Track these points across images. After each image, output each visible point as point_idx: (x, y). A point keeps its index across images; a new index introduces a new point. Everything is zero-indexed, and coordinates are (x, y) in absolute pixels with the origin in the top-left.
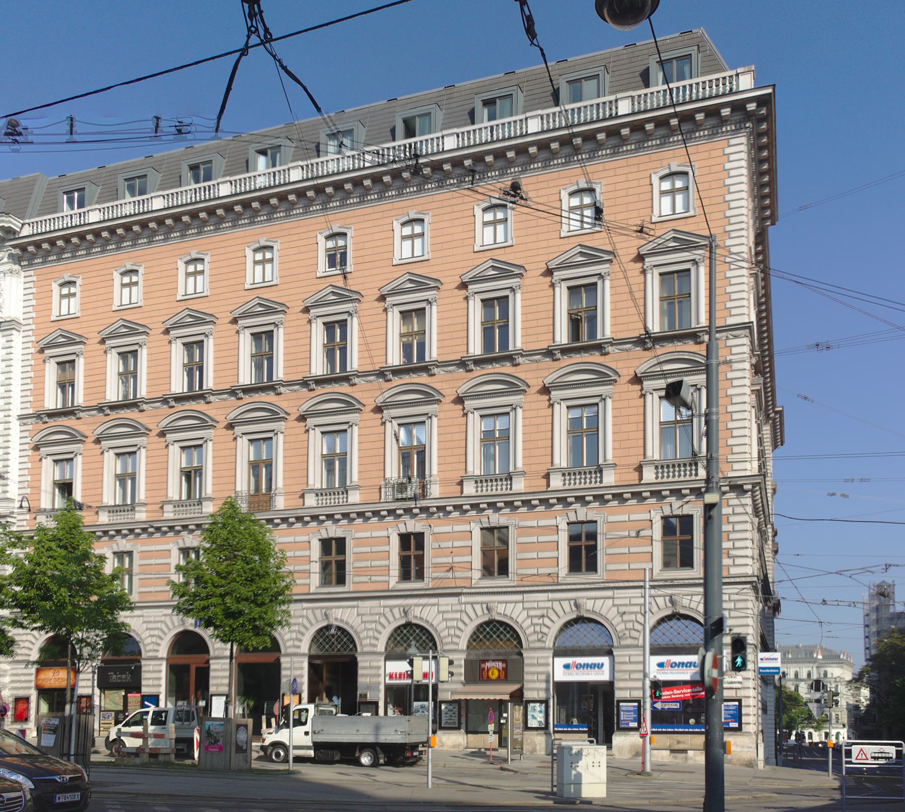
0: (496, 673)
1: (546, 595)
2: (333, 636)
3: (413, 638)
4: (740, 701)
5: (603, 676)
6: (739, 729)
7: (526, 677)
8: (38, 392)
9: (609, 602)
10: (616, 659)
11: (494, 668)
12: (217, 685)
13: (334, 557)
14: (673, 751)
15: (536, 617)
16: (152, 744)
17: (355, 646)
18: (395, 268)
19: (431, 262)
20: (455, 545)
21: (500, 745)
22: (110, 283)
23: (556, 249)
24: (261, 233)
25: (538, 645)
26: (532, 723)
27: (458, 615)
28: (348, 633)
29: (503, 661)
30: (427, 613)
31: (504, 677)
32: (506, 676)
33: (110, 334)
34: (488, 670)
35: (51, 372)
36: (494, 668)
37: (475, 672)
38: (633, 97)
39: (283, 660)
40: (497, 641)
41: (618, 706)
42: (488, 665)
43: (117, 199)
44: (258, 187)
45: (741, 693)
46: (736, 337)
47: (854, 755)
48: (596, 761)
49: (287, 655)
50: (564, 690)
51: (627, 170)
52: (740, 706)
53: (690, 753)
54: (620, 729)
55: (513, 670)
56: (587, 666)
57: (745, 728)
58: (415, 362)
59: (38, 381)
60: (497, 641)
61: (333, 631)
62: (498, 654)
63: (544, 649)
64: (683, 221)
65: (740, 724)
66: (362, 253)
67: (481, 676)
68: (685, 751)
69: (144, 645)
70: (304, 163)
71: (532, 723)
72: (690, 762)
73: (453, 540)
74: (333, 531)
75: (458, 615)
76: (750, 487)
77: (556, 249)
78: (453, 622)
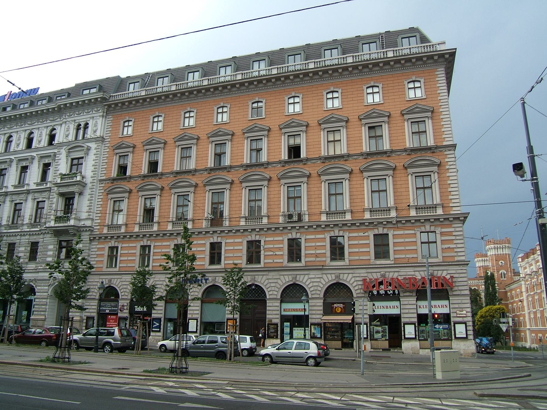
0: (340, 309)
1: (365, 270)
2: (254, 289)
3: (293, 292)
5: (396, 311)
8: (109, 169)
10: (278, 312)
11: (339, 307)
16: (245, 340)
19: (427, 100)
20: (315, 246)
22: (247, 107)
23: (321, 115)
29: (343, 303)
30: (304, 280)
31: (344, 312)
32: (345, 311)
34: (336, 308)
36: (339, 307)
37: (328, 309)
40: (337, 292)
44: (296, 69)
46: (450, 150)
50: (373, 318)
55: (349, 309)
58: (218, 168)
59: (109, 164)
60: (337, 292)
61: (253, 287)
64: (420, 101)
66: (146, 127)
67: (332, 311)
69: (301, 282)
74: (253, 237)
76: (463, 218)
77: (321, 115)
78: (316, 283)
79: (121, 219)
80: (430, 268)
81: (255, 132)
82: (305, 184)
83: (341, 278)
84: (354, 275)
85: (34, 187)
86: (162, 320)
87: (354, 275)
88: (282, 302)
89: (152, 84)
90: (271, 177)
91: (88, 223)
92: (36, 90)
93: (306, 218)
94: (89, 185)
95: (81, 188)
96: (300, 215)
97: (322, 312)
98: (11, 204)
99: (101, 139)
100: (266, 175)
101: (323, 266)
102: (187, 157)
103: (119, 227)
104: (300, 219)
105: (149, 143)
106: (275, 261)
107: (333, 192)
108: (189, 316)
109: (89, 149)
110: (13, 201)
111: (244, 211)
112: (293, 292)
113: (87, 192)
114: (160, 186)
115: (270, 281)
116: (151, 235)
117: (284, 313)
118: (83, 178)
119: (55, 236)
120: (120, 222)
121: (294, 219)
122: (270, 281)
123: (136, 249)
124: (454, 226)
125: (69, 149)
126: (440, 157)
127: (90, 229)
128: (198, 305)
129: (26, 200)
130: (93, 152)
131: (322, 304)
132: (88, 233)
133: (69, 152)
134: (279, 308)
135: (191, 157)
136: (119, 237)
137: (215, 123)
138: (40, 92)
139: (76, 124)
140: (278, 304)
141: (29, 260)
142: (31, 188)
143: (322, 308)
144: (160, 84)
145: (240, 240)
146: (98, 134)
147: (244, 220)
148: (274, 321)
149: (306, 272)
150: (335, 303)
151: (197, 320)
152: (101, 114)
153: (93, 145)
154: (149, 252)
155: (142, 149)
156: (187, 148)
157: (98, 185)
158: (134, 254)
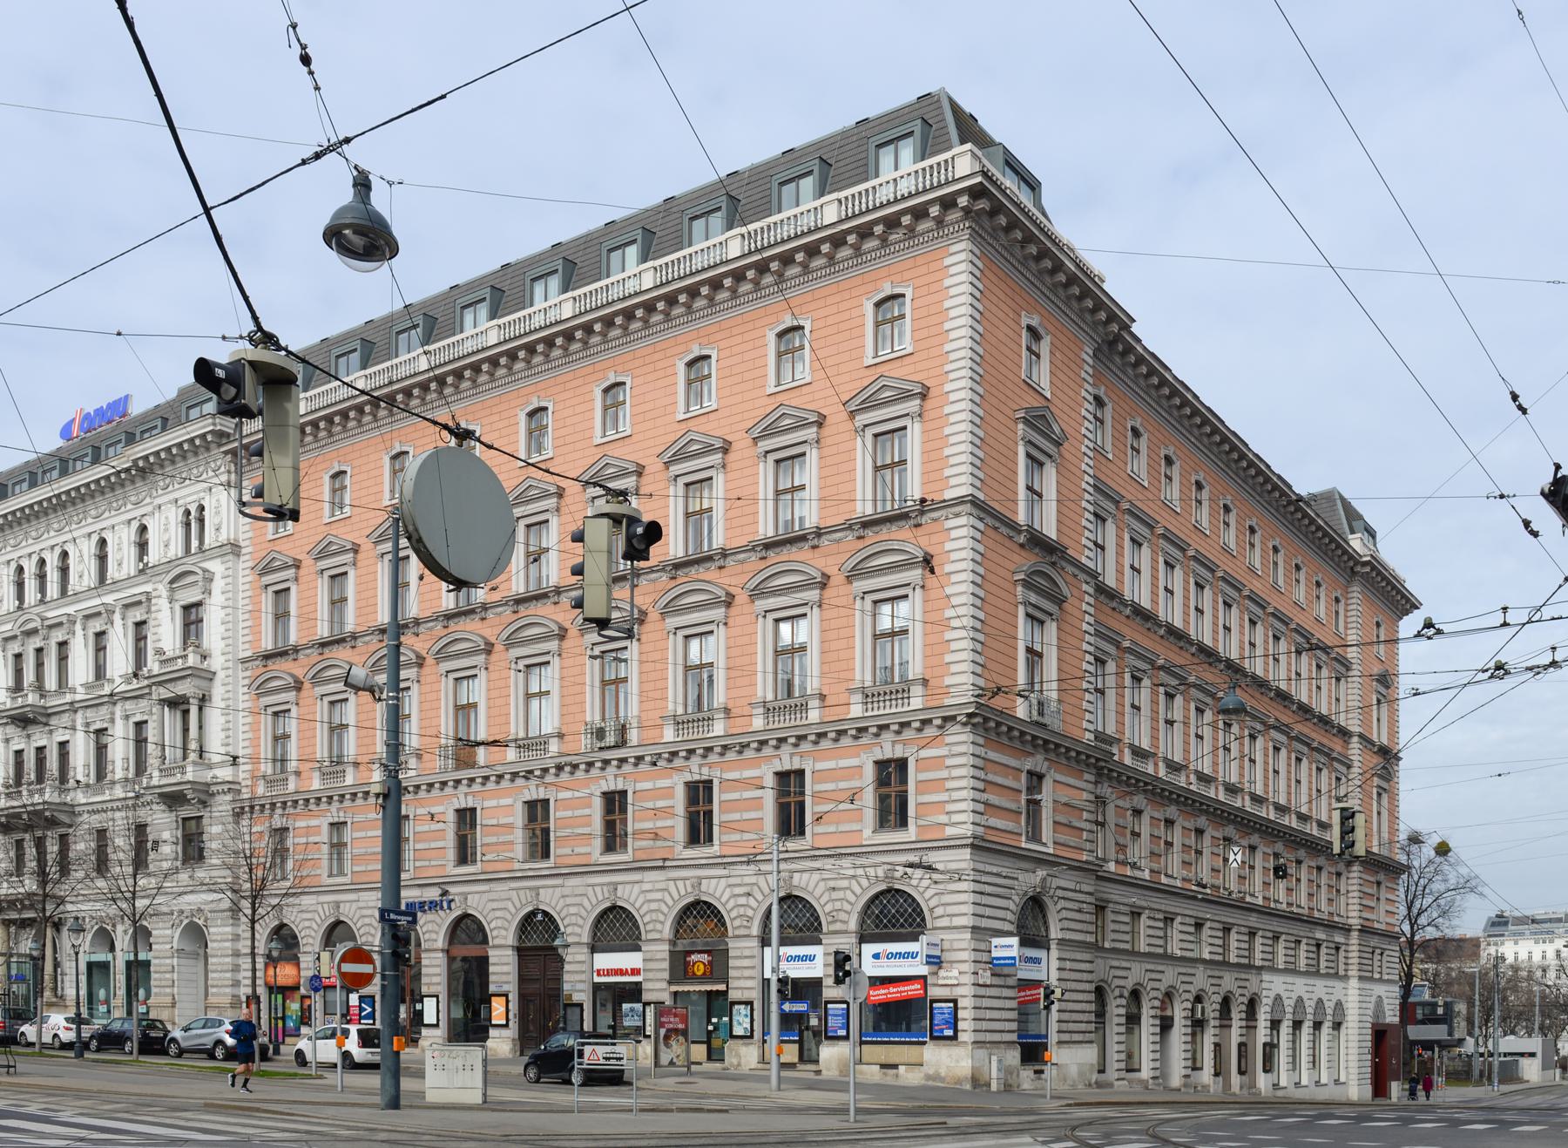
3: (616, 926)
4: (955, 1001)
6: (955, 1037)
7: (732, 973)
9: (816, 876)
12: (429, 984)
13: (893, 790)
14: (883, 1066)
15: (744, 897)
17: (923, 919)
18: (868, 372)
19: (634, 438)
21: (709, 1058)
24: (687, 339)
25: (742, 932)
26: (738, 1031)
27: (658, 896)
28: (914, 900)
29: (708, 952)
33: (863, 402)
35: (267, 601)
36: (699, 961)
38: (840, 201)
39: (491, 953)
41: (932, 1009)
42: (694, 957)
43: (867, 180)
45: (958, 991)
47: (587, 1055)
48: (468, 1064)
49: (494, 947)
51: (837, 298)
52: (956, 1008)
53: (902, 1069)
54: (828, 1038)
56: (900, 955)
57: (962, 1037)
61: (540, 917)
62: (707, 944)
63: (846, 932)
65: (956, 1031)
67: (686, 972)
68: (895, 1066)
70: (743, 230)
71: (738, 1031)
72: (901, 1082)
73: (655, 799)
75: (658, 896)
78: (655, 901)
79: (547, 718)
80: (783, 866)
81: (785, 436)
82: (918, 590)
83: (703, 888)
84: (732, 881)
85: (123, 688)
86: (378, 998)
87: (732, 881)
88: (594, 949)
89: (767, 206)
90: (826, 577)
91: (225, 773)
92: (120, 406)
93: (633, 736)
94: (221, 675)
95: (204, 684)
96: (623, 730)
97: (666, 975)
98: (126, 726)
99: (228, 549)
100: (814, 573)
101: (665, 860)
102: (893, 465)
103: (541, 742)
104: (622, 743)
105: (869, 405)
106: (577, 850)
107: (534, 689)
108: (492, 988)
109: (209, 578)
110: (127, 717)
111: (765, 689)
112: (616, 926)
113: (218, 692)
114: (920, 554)
115: (569, 900)
116: (904, 725)
117: (597, 979)
118: (204, 657)
119: (171, 808)
120: (548, 729)
121: (612, 739)
122: (569, 900)
123: (589, 806)
124: (949, 739)
125: (171, 582)
126: (935, 539)
127: (233, 787)
128: (438, 962)
129: (112, 721)
130: (218, 585)
131: (666, 955)
132: (229, 797)
133: (172, 590)
134: (756, 962)
135: (903, 462)
136: (904, 725)
137: (682, 417)
138: (136, 409)
139: (181, 510)
140: (757, 951)
141: (184, 862)
142: (78, 697)
143: (666, 965)
144: (887, 173)
145: (509, 801)
146: (223, 538)
147: (858, 697)
148: (576, 998)
149: (558, 881)
150: (693, 952)
151: (506, 996)
152: (224, 478)
153: (215, 566)
154: (802, 785)
155: (849, 426)
156: (540, 523)
157: (241, 675)
158: (668, 812)
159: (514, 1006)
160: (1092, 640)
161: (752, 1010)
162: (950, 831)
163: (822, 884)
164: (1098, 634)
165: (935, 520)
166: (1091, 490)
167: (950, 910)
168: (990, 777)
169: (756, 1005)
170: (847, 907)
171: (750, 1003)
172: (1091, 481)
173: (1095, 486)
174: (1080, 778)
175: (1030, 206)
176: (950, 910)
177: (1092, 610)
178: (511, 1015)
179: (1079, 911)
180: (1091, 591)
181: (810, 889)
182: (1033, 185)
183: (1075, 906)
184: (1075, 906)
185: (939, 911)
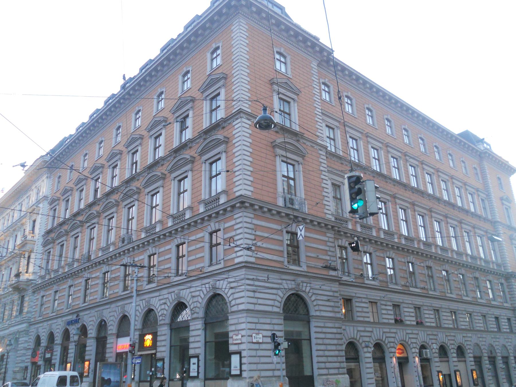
6: (240, 375)
45: (242, 347)
84: (161, 297)
87: (161, 297)
124: (235, 216)
126: (230, 131)
159: (202, 364)
160: (327, 174)
161: (198, 361)
162: (237, 261)
163: (190, 294)
164: (329, 171)
165: (229, 124)
166: (320, 114)
167: (238, 301)
168: (258, 233)
169: (200, 358)
170: (199, 305)
171: (197, 357)
172: (320, 111)
173: (322, 113)
174: (325, 236)
175: (280, 14)
176: (238, 301)
177: (325, 162)
178: (90, 371)
179: (328, 300)
180: (324, 154)
181: (186, 298)
182: (282, 8)
183: (325, 298)
184: (325, 298)
185: (233, 303)
